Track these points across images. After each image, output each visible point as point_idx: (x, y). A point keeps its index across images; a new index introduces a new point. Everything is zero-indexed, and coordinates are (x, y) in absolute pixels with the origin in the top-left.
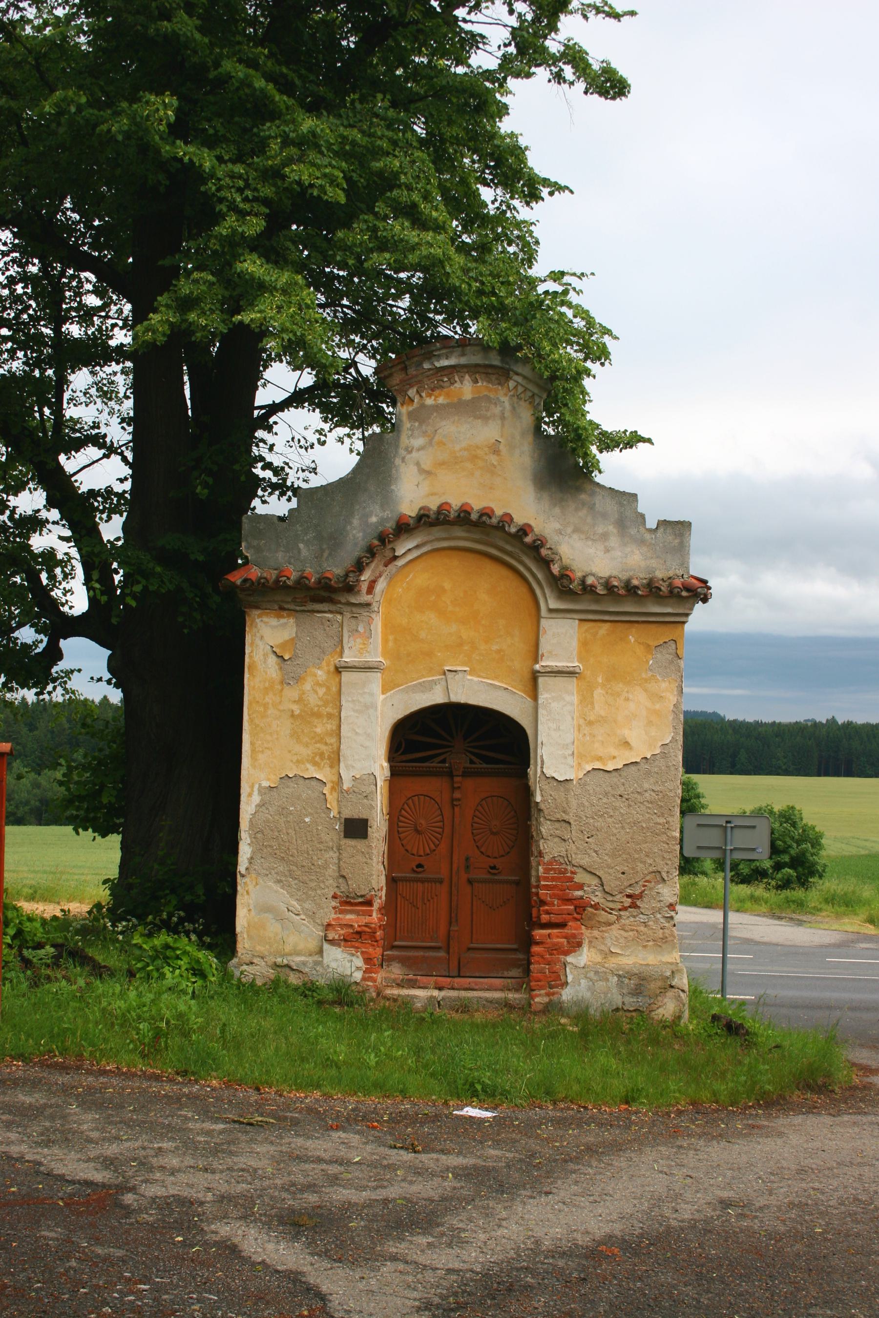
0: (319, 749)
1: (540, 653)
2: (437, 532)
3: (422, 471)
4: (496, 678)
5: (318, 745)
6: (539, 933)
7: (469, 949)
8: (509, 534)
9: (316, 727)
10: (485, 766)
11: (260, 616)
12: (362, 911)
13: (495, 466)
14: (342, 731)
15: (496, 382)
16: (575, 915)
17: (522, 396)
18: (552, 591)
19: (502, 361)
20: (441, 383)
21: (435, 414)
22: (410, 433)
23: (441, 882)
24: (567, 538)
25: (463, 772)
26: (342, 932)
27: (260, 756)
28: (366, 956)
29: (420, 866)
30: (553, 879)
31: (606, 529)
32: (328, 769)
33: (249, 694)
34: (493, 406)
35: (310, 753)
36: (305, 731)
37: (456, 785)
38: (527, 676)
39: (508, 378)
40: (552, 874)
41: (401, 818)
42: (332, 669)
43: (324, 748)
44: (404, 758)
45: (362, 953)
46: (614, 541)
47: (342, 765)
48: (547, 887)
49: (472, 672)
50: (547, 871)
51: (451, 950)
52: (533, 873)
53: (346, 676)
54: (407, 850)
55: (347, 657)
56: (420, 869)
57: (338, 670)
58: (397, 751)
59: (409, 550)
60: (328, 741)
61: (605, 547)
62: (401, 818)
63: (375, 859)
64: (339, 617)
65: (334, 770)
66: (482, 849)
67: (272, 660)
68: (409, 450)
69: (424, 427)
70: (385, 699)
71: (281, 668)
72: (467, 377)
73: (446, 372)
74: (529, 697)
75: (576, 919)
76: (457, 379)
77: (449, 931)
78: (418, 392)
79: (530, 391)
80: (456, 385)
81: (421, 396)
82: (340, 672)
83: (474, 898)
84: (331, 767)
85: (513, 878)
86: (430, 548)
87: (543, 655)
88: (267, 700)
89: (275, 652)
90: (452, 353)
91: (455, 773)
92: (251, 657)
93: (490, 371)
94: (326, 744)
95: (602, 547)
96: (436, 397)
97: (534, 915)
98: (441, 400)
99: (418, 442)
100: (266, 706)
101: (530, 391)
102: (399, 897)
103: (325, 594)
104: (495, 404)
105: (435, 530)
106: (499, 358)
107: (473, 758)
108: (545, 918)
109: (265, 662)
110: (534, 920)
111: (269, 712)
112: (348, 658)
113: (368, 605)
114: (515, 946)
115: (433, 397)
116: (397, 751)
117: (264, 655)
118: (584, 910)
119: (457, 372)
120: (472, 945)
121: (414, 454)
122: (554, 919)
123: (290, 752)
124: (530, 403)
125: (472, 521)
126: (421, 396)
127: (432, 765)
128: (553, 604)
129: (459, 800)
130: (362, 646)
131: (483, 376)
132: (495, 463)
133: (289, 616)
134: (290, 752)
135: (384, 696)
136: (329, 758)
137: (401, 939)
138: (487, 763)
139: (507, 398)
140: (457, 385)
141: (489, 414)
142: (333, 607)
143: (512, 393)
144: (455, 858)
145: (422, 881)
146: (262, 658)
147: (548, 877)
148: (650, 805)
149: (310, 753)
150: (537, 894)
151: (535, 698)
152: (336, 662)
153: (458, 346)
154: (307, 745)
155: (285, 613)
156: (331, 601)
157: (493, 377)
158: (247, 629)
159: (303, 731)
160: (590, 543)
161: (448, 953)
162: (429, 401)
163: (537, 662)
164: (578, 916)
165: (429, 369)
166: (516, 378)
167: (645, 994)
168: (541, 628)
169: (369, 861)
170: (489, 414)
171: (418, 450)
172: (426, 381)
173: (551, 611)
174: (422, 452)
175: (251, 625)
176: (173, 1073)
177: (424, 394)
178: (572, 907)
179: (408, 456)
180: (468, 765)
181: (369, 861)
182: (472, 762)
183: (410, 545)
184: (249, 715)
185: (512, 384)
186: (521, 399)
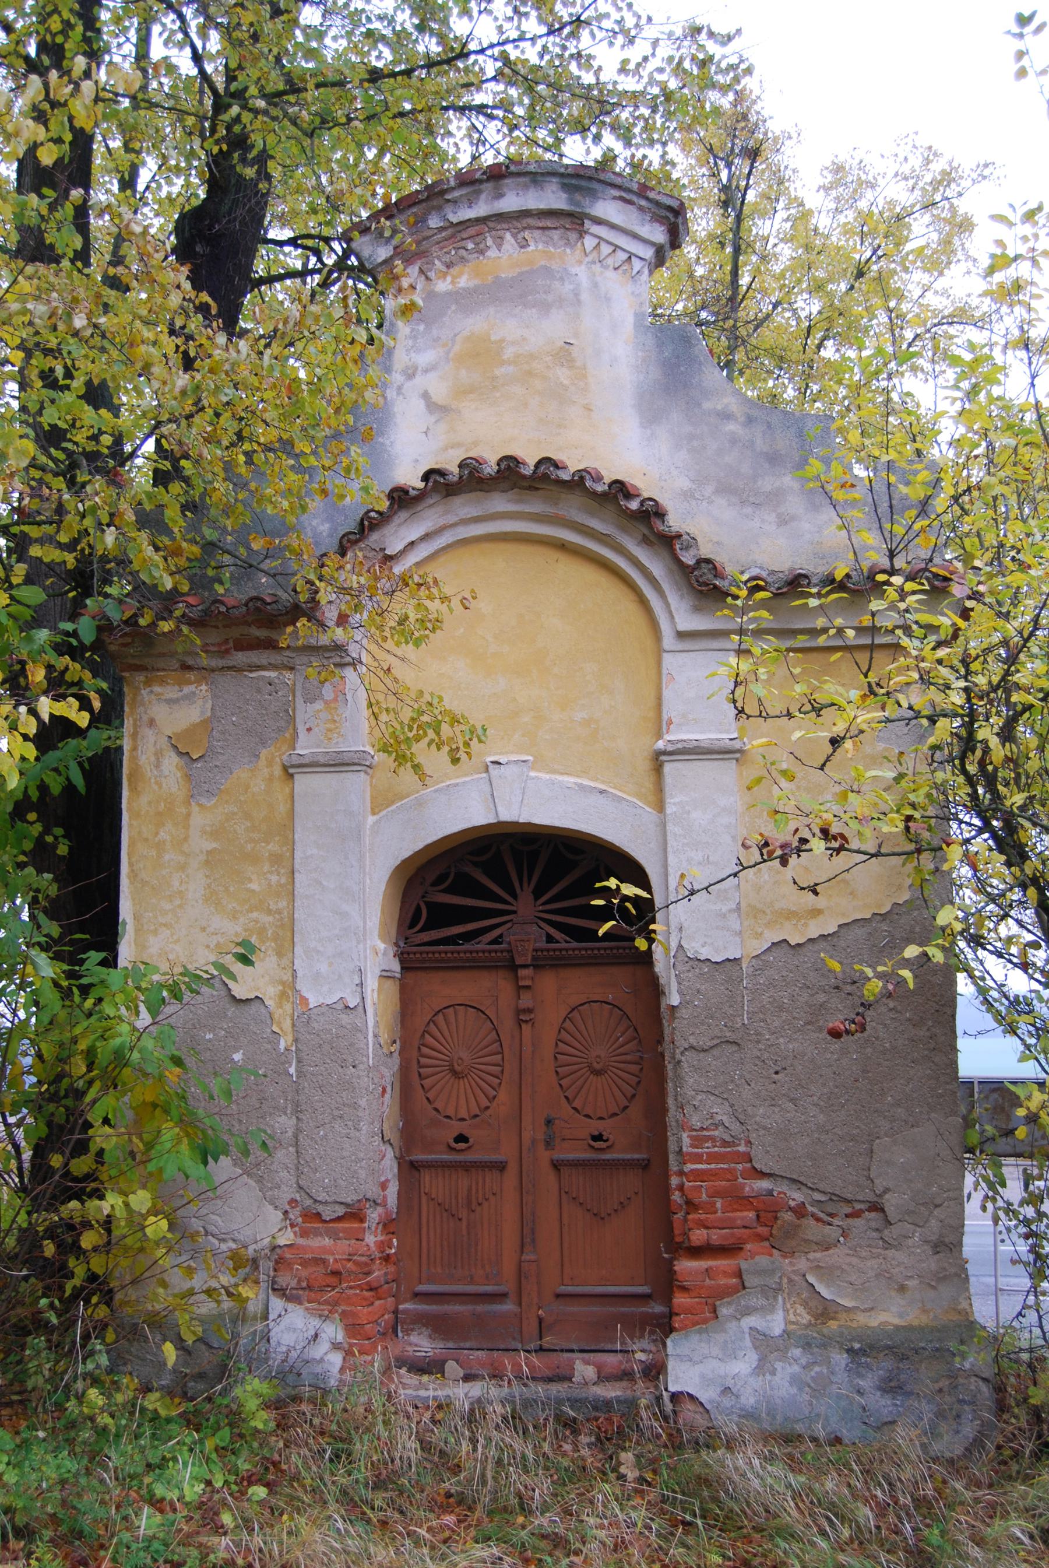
0: (257, 922)
1: (665, 717)
2: (463, 507)
3: (432, 406)
4: (584, 773)
5: (255, 915)
6: (686, 1266)
7: (558, 1296)
8: (595, 494)
9: (250, 880)
10: (574, 944)
11: (148, 683)
12: (344, 1230)
13: (566, 388)
14: (297, 885)
15: (562, 243)
16: (761, 1230)
17: (610, 261)
18: (682, 597)
19: (571, 201)
20: (462, 252)
21: (454, 307)
22: (410, 342)
23: (501, 1167)
24: (705, 503)
25: (534, 958)
26: (304, 1273)
27: (151, 940)
28: (350, 1321)
29: (461, 1138)
30: (713, 1158)
31: (778, 484)
32: (274, 959)
33: (130, 825)
34: (557, 284)
35: (239, 929)
36: (232, 889)
37: (521, 983)
38: (643, 765)
39: (582, 233)
40: (708, 1148)
41: (425, 1050)
42: (278, 771)
43: (267, 919)
44: (426, 937)
45: (344, 1315)
46: (795, 504)
47: (298, 949)
48: (698, 1175)
49: (539, 764)
50: (697, 1141)
51: (525, 1300)
52: (672, 1146)
53: (304, 783)
54: (436, 1110)
55: (302, 748)
56: (462, 1145)
57: (287, 774)
58: (412, 926)
59: (412, 543)
60: (273, 907)
61: (779, 516)
62: (425, 1050)
63: (364, 1127)
64: (288, 675)
65: (285, 962)
66: (576, 1104)
67: (171, 762)
68: (410, 374)
69: (435, 332)
70: (378, 822)
71: (188, 777)
72: (508, 236)
73: (472, 231)
74: (649, 804)
75: (761, 1238)
76: (489, 242)
77: (520, 1261)
78: (421, 271)
79: (624, 250)
80: (489, 253)
81: (427, 278)
82: (292, 776)
83: (564, 1196)
84: (280, 954)
85: (636, 1156)
86: (451, 540)
87: (670, 722)
88: (162, 835)
89: (175, 747)
90: (478, 192)
91: (519, 961)
92: (134, 759)
93: (549, 223)
94: (269, 912)
95: (772, 517)
96: (454, 278)
97: (677, 1232)
98: (463, 282)
99: (425, 358)
100: (160, 846)
101: (624, 250)
102: (424, 1199)
103: (261, 633)
104: (562, 279)
105: (457, 501)
106: (564, 196)
107: (552, 931)
108: (699, 1236)
109: (158, 766)
110: (678, 1239)
111: (167, 857)
112: (305, 748)
113: (338, 648)
114: (645, 1289)
115: (449, 279)
116: (412, 926)
117: (156, 754)
118: (776, 1218)
119: (491, 229)
120: (563, 1289)
121: (419, 380)
122: (716, 1237)
123: (203, 929)
124: (625, 272)
125: (524, 477)
126: (427, 278)
127: (479, 947)
128: (688, 622)
129: (529, 1011)
130: (329, 726)
131: (537, 233)
132: (566, 382)
133: (198, 682)
134: (203, 929)
135: (375, 818)
136: (276, 938)
137: (430, 1280)
138: (578, 941)
139: (583, 267)
140: (492, 253)
141: (550, 298)
142: (274, 658)
143: (589, 259)
144: (527, 1119)
145: (467, 1167)
146: (153, 759)
147: (700, 1155)
148: (481, 1440)
149: (239, 929)
150: (681, 1188)
151: (660, 806)
152: (285, 757)
153: (488, 180)
154: (234, 917)
155: (192, 676)
156: (271, 645)
157: (556, 235)
158: (126, 709)
159: (227, 890)
160: (748, 510)
161: (520, 1304)
162: (442, 286)
163: (659, 736)
164: (762, 1230)
165: (441, 229)
166: (596, 229)
167: (908, 1388)
168: (664, 672)
169: (353, 1133)
170: (550, 298)
171: (426, 371)
172: (435, 251)
173: (681, 635)
174: (432, 375)
175: (134, 700)
176: (115, 1499)
177: (431, 274)
178: (752, 1215)
179: (408, 385)
180: (542, 944)
181: (353, 1133)
182: (550, 939)
183: (414, 532)
184: (131, 864)
185: (589, 242)
186: (607, 267)
